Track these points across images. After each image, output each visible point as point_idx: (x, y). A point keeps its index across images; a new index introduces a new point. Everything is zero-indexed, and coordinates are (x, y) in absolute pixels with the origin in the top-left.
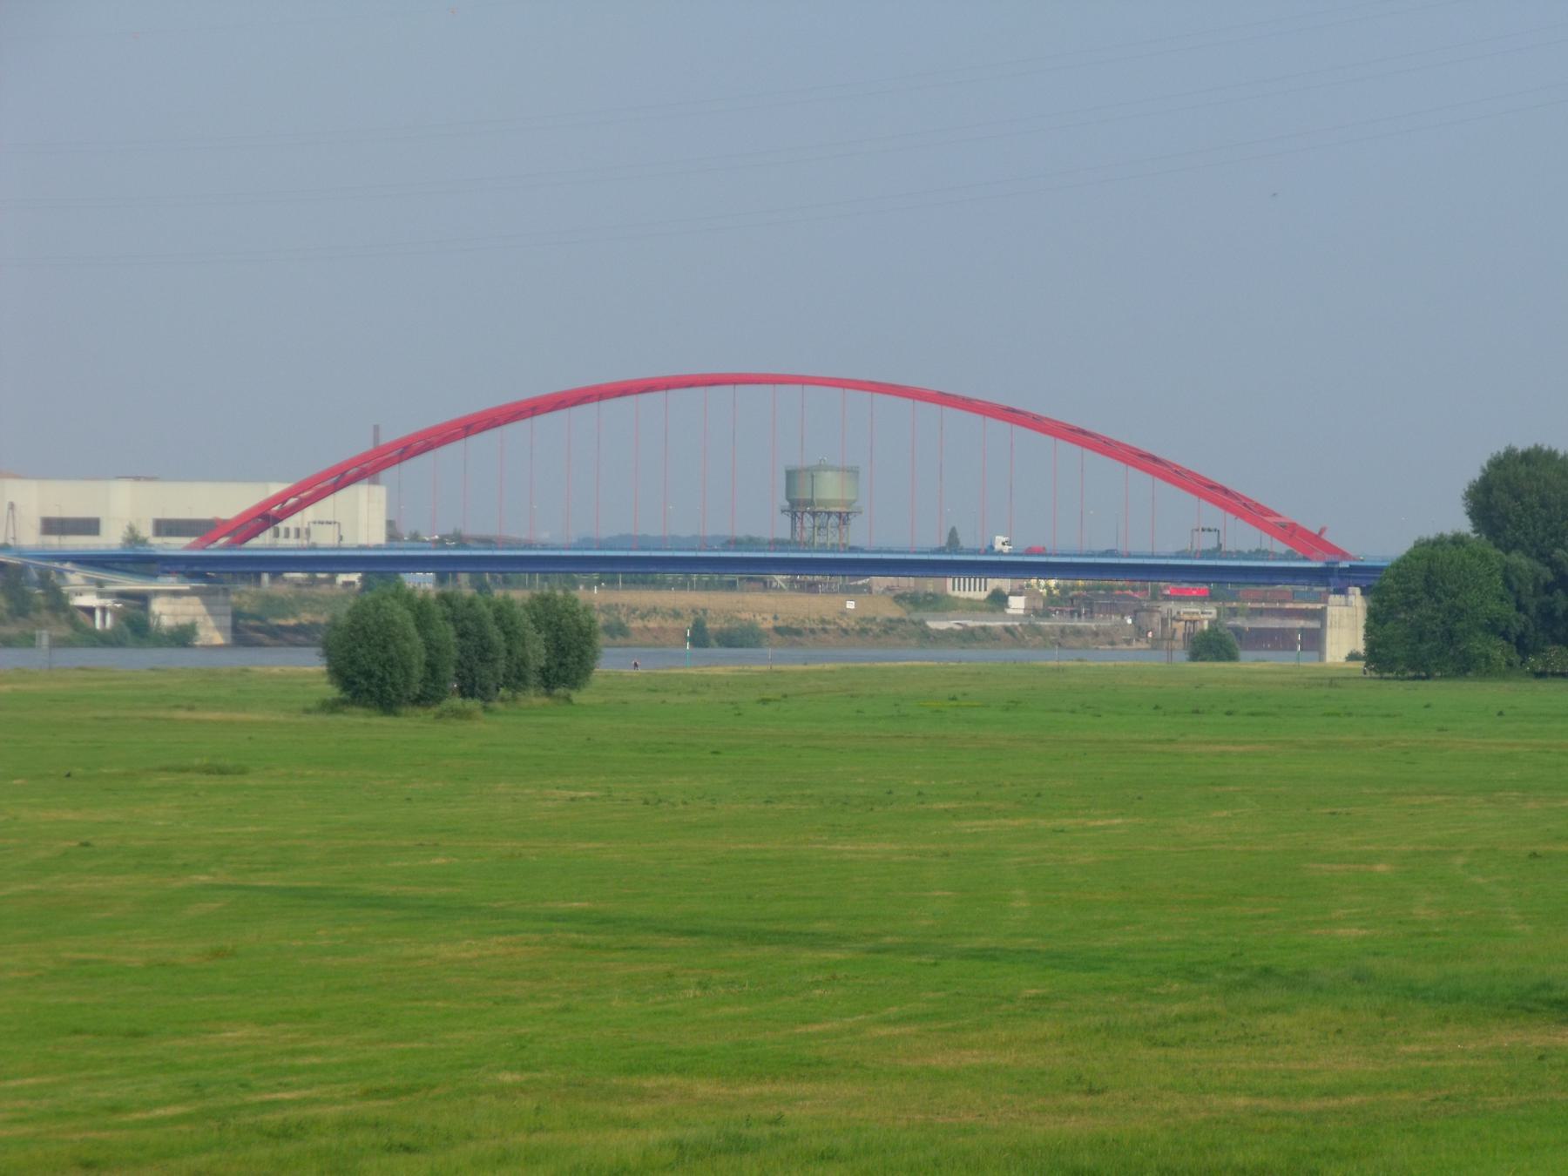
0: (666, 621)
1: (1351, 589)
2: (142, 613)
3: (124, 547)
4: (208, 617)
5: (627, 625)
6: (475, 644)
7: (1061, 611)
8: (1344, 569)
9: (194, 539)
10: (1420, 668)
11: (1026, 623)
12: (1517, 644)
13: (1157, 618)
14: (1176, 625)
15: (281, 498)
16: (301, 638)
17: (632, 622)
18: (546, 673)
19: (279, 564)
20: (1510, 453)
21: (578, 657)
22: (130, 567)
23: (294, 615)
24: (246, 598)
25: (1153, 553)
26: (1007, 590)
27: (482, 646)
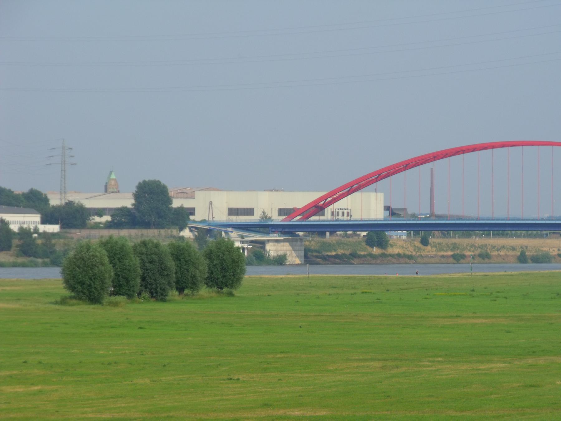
0: (509, 252)
4: (293, 252)
6: (158, 267)
16: (337, 260)
17: (493, 252)
18: (217, 281)
19: (333, 228)
21: (233, 272)
22: (262, 230)
23: (335, 250)
24: (313, 243)
25: (362, 219)
27: (161, 268)
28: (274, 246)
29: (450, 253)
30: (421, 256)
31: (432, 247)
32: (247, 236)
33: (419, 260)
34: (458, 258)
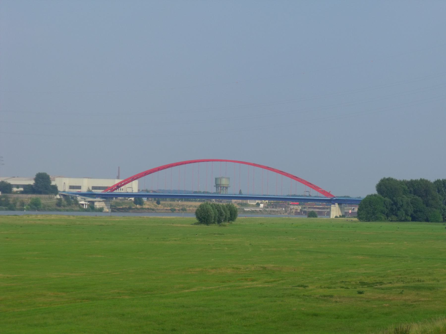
1: (336, 204)
2: (93, 205)
3: (87, 192)
4: (106, 206)
5: (186, 209)
7: (270, 207)
8: (335, 199)
9: (103, 190)
10: (368, 220)
11: (263, 209)
12: (386, 215)
13: (289, 209)
14: (293, 210)
15: (121, 183)
16: (123, 211)
19: (117, 196)
20: (384, 178)
23: (122, 206)
24: (112, 202)
26: (260, 203)
27: (221, 213)
28: (98, 203)
29: (169, 208)
30: (158, 209)
31: (161, 205)
32: (86, 199)
33: (157, 211)
34: (173, 210)
